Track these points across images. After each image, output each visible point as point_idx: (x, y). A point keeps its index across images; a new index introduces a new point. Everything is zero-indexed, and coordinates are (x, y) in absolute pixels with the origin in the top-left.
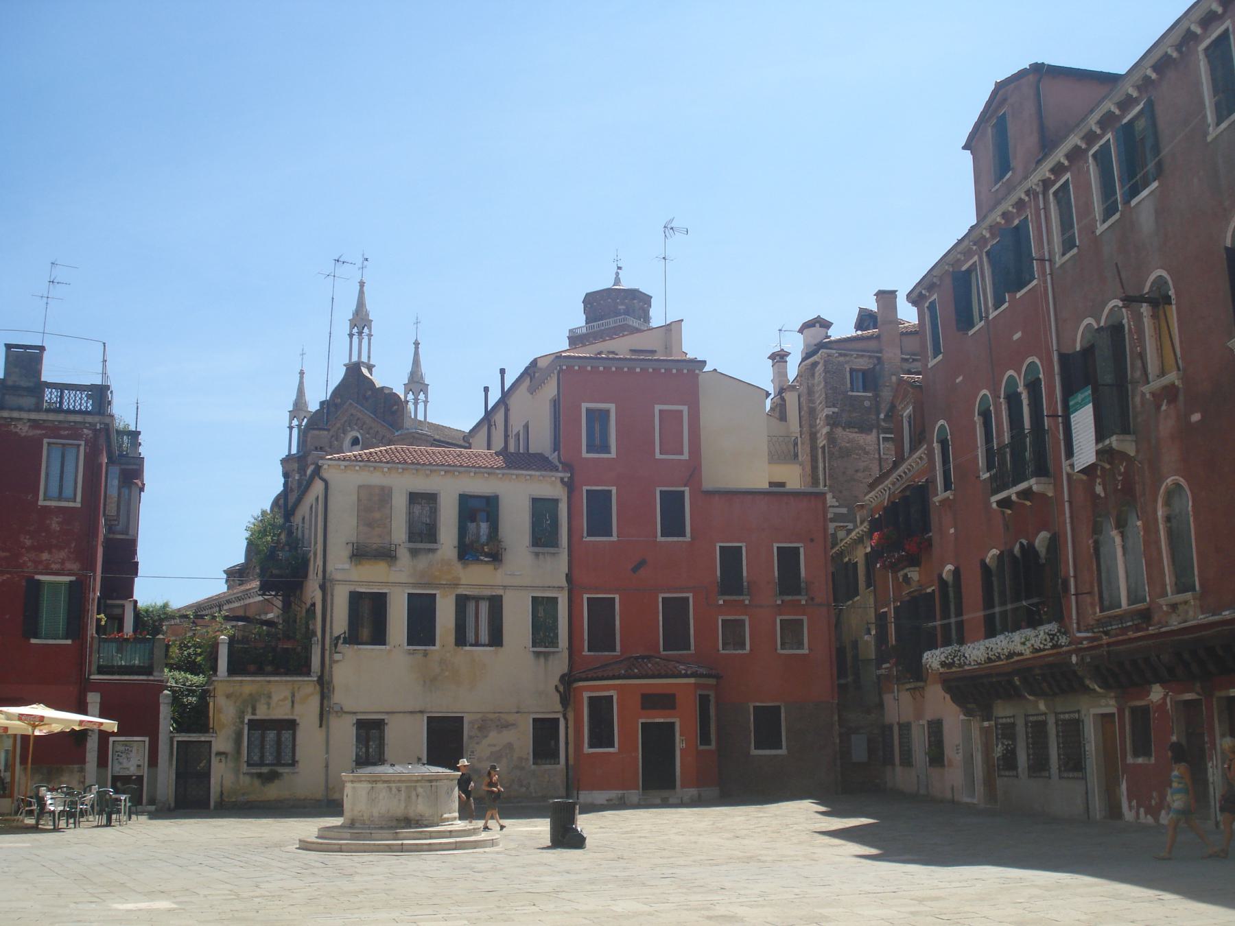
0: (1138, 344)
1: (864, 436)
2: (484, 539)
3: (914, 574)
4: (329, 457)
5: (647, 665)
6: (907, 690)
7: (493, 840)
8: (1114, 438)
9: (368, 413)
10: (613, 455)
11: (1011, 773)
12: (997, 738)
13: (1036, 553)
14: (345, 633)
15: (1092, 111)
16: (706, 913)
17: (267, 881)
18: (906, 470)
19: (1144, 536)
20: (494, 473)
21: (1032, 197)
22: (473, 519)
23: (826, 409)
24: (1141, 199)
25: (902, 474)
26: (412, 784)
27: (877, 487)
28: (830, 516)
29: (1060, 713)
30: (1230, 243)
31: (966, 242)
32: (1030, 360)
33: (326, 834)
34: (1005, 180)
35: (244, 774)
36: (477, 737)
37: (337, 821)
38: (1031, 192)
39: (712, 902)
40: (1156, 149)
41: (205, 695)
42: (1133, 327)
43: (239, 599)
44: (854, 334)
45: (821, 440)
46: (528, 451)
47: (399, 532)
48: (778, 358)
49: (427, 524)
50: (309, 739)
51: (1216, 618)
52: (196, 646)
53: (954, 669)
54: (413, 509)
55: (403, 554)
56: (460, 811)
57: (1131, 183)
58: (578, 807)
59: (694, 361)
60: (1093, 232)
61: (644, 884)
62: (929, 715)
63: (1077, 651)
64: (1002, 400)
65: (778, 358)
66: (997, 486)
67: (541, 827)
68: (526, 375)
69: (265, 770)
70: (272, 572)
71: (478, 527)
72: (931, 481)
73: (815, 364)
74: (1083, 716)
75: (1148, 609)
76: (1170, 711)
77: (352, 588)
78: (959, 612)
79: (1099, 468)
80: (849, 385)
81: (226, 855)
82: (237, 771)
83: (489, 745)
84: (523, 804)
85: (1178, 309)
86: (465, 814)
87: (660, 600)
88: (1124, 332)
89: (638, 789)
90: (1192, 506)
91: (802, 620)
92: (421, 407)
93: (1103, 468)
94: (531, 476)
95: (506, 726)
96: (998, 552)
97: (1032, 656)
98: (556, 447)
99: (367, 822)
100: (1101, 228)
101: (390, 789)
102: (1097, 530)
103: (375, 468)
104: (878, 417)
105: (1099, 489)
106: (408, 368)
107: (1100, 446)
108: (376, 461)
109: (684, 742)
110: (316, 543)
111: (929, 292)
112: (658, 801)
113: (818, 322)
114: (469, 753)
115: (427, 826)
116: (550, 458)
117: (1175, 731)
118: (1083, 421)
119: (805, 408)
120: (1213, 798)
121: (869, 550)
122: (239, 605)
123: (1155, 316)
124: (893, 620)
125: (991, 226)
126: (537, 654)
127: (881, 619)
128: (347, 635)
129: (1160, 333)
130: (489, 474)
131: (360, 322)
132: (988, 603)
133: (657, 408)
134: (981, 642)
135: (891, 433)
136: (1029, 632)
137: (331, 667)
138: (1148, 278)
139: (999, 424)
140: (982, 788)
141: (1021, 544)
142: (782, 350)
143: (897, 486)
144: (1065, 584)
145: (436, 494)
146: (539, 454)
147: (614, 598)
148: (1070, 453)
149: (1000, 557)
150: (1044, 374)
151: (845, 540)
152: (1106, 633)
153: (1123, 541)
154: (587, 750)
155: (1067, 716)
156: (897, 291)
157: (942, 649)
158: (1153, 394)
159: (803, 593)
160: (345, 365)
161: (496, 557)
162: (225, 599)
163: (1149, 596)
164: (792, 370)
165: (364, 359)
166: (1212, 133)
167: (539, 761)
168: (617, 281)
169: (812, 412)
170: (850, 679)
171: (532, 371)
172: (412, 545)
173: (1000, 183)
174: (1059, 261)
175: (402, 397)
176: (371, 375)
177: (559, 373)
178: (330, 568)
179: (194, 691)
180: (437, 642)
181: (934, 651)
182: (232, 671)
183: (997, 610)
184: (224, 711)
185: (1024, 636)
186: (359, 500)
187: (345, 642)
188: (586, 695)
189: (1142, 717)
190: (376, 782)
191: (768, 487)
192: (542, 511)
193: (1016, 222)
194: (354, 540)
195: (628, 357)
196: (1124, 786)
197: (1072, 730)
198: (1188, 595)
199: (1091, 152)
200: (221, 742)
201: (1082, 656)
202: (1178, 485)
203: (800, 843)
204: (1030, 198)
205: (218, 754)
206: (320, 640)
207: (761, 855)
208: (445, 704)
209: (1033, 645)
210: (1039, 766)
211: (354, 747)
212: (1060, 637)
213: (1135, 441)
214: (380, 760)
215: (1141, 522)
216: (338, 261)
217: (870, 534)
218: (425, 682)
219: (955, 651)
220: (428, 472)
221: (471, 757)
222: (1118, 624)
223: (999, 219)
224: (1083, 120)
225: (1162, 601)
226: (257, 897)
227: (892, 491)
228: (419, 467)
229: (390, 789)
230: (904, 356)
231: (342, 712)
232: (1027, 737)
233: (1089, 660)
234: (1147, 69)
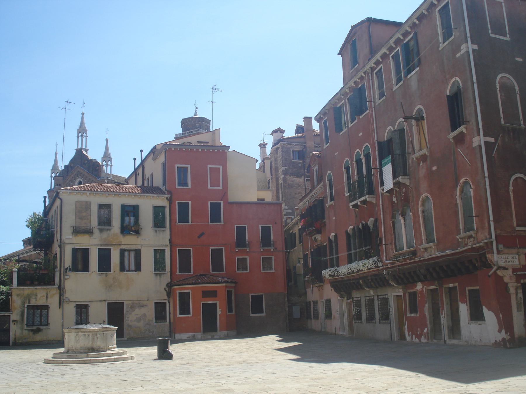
0: (410, 137)
1: (298, 179)
2: (132, 224)
3: (319, 237)
4: (63, 189)
5: (204, 278)
6: (317, 287)
7: (131, 357)
8: (400, 177)
9: (86, 170)
10: (189, 187)
11: (359, 321)
12: (353, 307)
13: (368, 227)
14: (70, 266)
15: (391, 37)
16: (218, 388)
17: (25, 379)
18: (315, 193)
19: (413, 219)
20: (137, 195)
21: (366, 75)
22: (128, 215)
23: (282, 168)
24: (411, 75)
25: (313, 195)
26: (95, 333)
27: (303, 200)
28: (283, 213)
29: (379, 295)
30: (449, 93)
31: (339, 94)
32: (366, 145)
33: (56, 356)
34: (355, 68)
35: (25, 330)
36: (130, 311)
37: (62, 350)
38: (366, 73)
39: (221, 383)
40: (418, 53)
41: (8, 295)
42: (408, 130)
43: (27, 252)
44: (294, 136)
45: (280, 181)
46: (152, 186)
47: (94, 221)
48: (262, 146)
49: (107, 218)
50: (54, 313)
51: (443, 254)
52: (5, 273)
53: (335, 277)
54: (100, 211)
55: (96, 231)
56: (117, 344)
57: (408, 68)
58: (169, 341)
59: (225, 146)
60: (392, 89)
61: (195, 375)
62: (325, 298)
63: (386, 269)
64: (354, 162)
65: (262, 146)
66: (352, 198)
67: (154, 350)
68: (151, 153)
69: (35, 328)
70: (38, 240)
71: (130, 219)
72: (325, 197)
73: (278, 148)
74: (389, 296)
75: (415, 250)
76: (425, 294)
77: (73, 246)
78: (337, 253)
79: (394, 190)
81: (10, 367)
82: (22, 329)
83: (136, 315)
84: (151, 340)
85: (427, 122)
86: (119, 346)
87: (210, 250)
88: (405, 132)
89: (201, 332)
90: (433, 206)
91: (272, 258)
92: (109, 167)
93: (396, 191)
94: (153, 196)
95: (143, 306)
96: (353, 227)
97: (367, 271)
98: (164, 184)
99: (75, 350)
100: (395, 88)
101: (85, 335)
102: (393, 217)
103: (83, 193)
104: (305, 171)
105: (394, 200)
106: (103, 150)
107: (395, 181)
108: (84, 190)
109: (221, 311)
110: (57, 227)
111: (324, 116)
112: (210, 337)
113: (279, 130)
114: (126, 318)
115: (102, 351)
116: (162, 189)
117: (427, 302)
118: (388, 170)
119: (274, 167)
120: (443, 331)
121: (300, 227)
122: (27, 255)
123: (417, 125)
124: (310, 257)
125: (349, 88)
126: (156, 274)
127: (305, 256)
128: (71, 267)
129: (420, 132)
130: (134, 196)
131: (82, 131)
132: (349, 249)
133: (209, 166)
134: (346, 265)
135: (309, 178)
136: (366, 261)
137: (64, 282)
138: (415, 108)
139: (353, 173)
140: (347, 328)
141: (362, 224)
142: (264, 142)
143: (311, 200)
144: (381, 239)
145: (111, 205)
146: (157, 187)
147: (190, 249)
148: (382, 184)
149: (354, 229)
150: (371, 151)
151: (291, 223)
152: (398, 261)
153: (404, 221)
154: (178, 316)
155: (382, 297)
156: (312, 117)
157: (330, 269)
158: (417, 158)
159: (272, 246)
160: (75, 150)
161: (138, 232)
162: (21, 253)
163: (416, 244)
164: (268, 151)
165: (84, 147)
166: (442, 46)
167: (158, 321)
168: (196, 114)
169: (277, 169)
170: (293, 282)
171: (154, 150)
172: (100, 227)
173: (353, 69)
174: (378, 102)
175: (101, 163)
176: (87, 154)
177: (165, 152)
178: (63, 238)
179: (4, 293)
180: (112, 270)
181: (326, 270)
182: (20, 284)
183: (353, 252)
184: (16, 302)
185: (363, 263)
186: (76, 208)
187: (70, 270)
188: (178, 292)
189: (413, 296)
190: (78, 332)
192: (158, 212)
193: (360, 86)
194: (74, 225)
195: (196, 144)
196: (406, 326)
197: (384, 302)
198: (432, 244)
199: (391, 56)
200: (14, 316)
201: (388, 271)
202: (427, 197)
203: (268, 354)
204: (366, 75)
205: (14, 321)
206: (59, 269)
207: (249, 360)
208: (115, 297)
209: (367, 267)
210: (371, 318)
211: (75, 317)
212: (379, 263)
213: (409, 179)
214: (87, 322)
215: (412, 213)
216: (67, 102)
217: (300, 221)
218: (106, 287)
219: (335, 270)
220: (107, 195)
221: (128, 320)
222: (402, 257)
223: (353, 85)
224: (388, 41)
225: (421, 247)
226: (18, 386)
227: (309, 202)
228: (103, 193)
229: (85, 335)
230: (315, 145)
231: (69, 301)
232: (366, 306)
233: (391, 272)
234: (414, 19)
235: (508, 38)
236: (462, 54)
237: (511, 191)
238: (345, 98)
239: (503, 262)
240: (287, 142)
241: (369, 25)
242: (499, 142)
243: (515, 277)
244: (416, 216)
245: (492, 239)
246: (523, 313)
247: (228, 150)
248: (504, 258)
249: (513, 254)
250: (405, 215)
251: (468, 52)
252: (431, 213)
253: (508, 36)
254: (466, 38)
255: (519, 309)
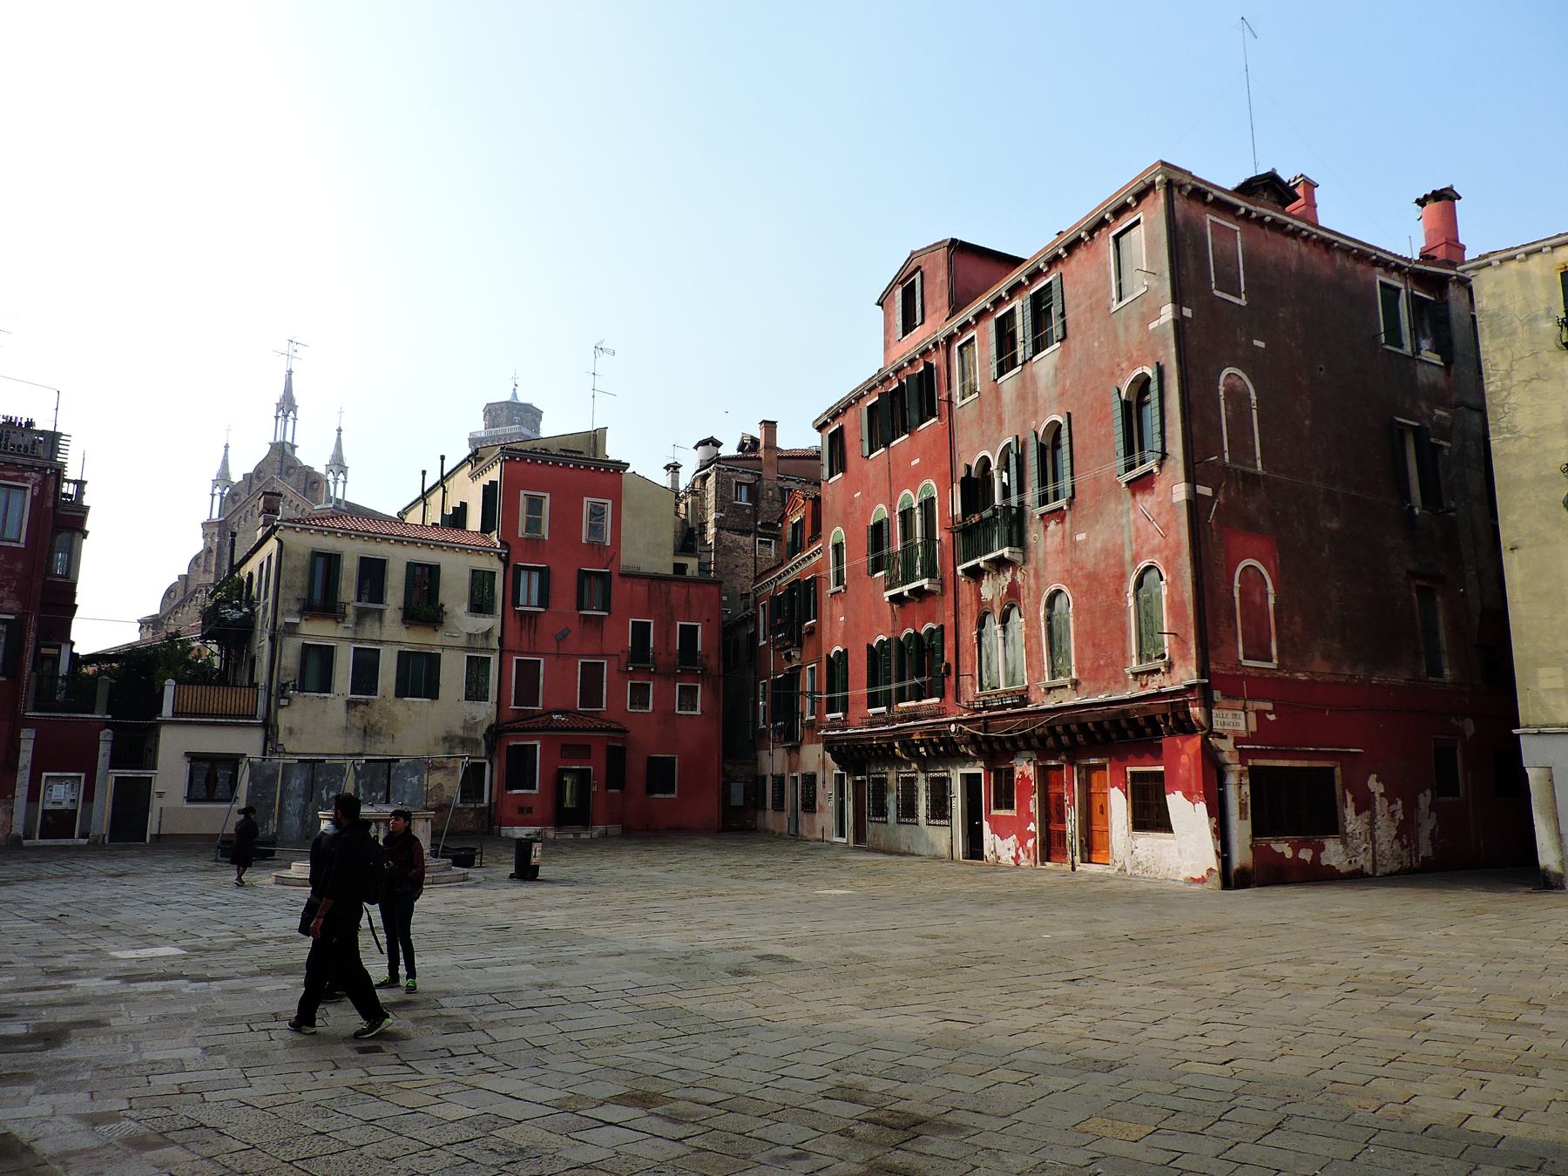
1: (744, 538)
44: (736, 454)
80: (734, 496)
92: (340, 485)
106: (331, 450)
131: (287, 405)
137: (276, 712)
165: (289, 439)
191: (672, 573)
192: (480, 580)
235: (1242, 302)
246: (1249, 822)
247: (624, 471)
252: (1067, 622)
255: (1242, 816)
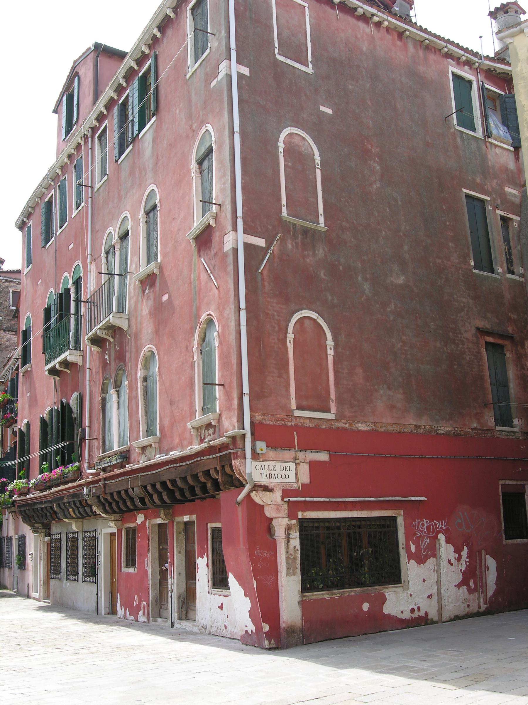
102: (104, 390)
201: (90, 487)
235: (310, 70)
236: (219, 80)
237: (290, 341)
238: (56, 186)
239: (264, 476)
240: (5, 277)
241: (98, 56)
242: (275, 247)
243: (286, 506)
244: (132, 388)
245: (244, 429)
246: (298, 577)
248: (267, 468)
249: (284, 461)
250: (120, 386)
251: (229, 77)
253: (310, 65)
254: (229, 49)
